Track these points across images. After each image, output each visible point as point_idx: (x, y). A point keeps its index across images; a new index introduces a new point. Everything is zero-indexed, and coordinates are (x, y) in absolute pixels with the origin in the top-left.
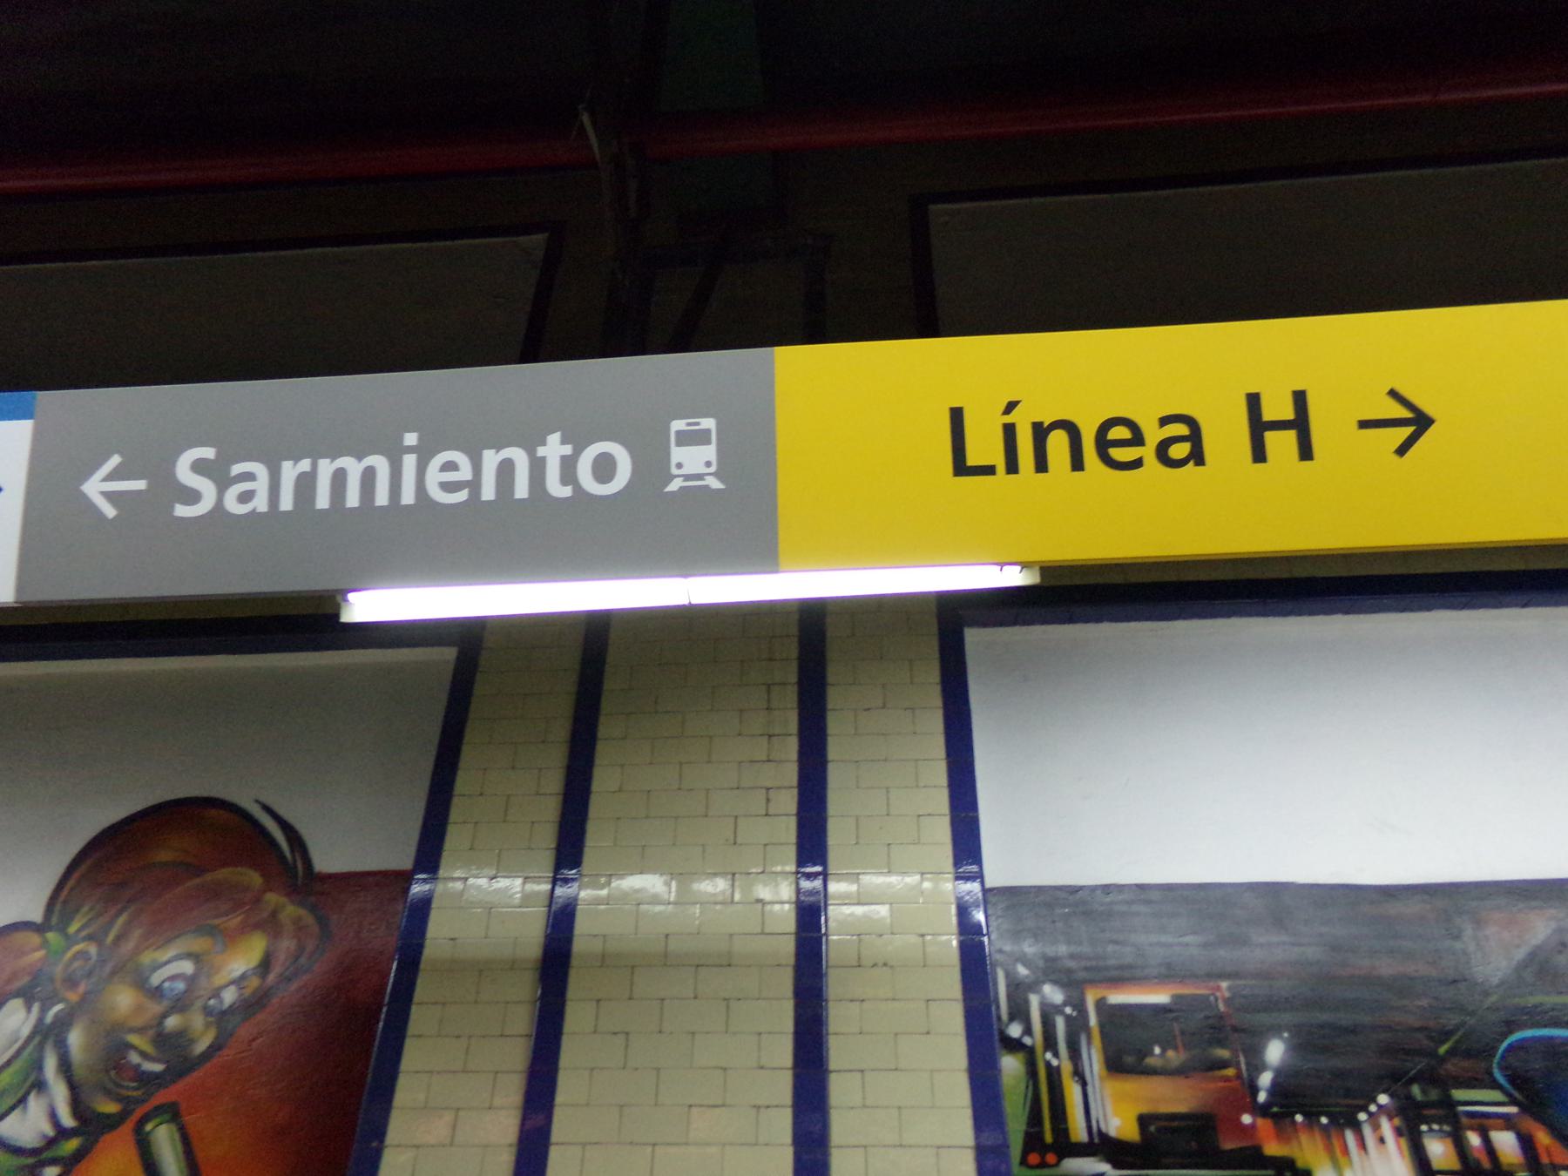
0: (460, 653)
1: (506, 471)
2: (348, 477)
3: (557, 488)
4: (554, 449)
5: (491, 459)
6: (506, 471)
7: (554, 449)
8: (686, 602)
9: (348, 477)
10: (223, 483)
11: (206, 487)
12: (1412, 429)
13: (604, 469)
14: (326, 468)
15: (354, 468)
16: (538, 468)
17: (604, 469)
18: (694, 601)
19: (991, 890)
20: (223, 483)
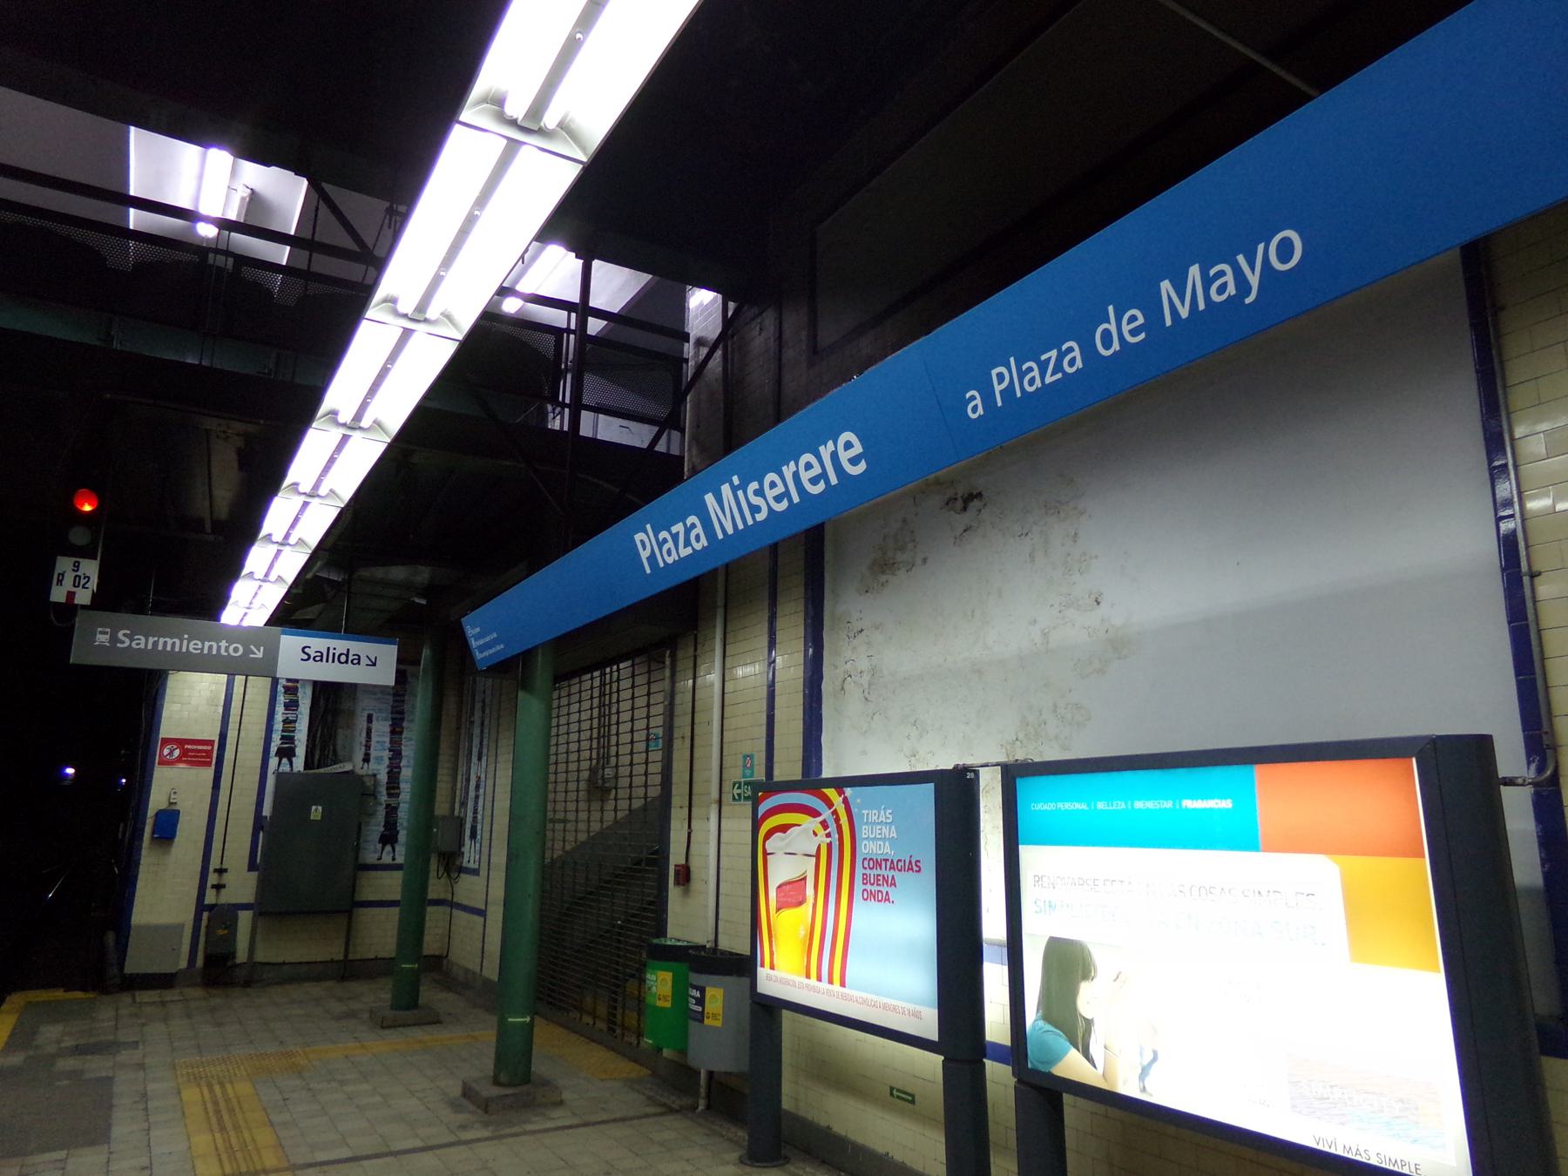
0: (218, 620)
1: (210, 647)
2: (168, 643)
3: (223, 653)
4: (223, 644)
5: (151, 640)
6: (210, 647)
7: (223, 644)
8: (1560, 1153)
9: (168, 643)
10: (132, 640)
11: (127, 642)
12: (324, 185)
13: (236, 650)
14: (162, 640)
15: (170, 641)
16: (219, 648)
17: (236, 650)
18: (1562, 1162)
19: (806, 772)
20: (132, 640)
